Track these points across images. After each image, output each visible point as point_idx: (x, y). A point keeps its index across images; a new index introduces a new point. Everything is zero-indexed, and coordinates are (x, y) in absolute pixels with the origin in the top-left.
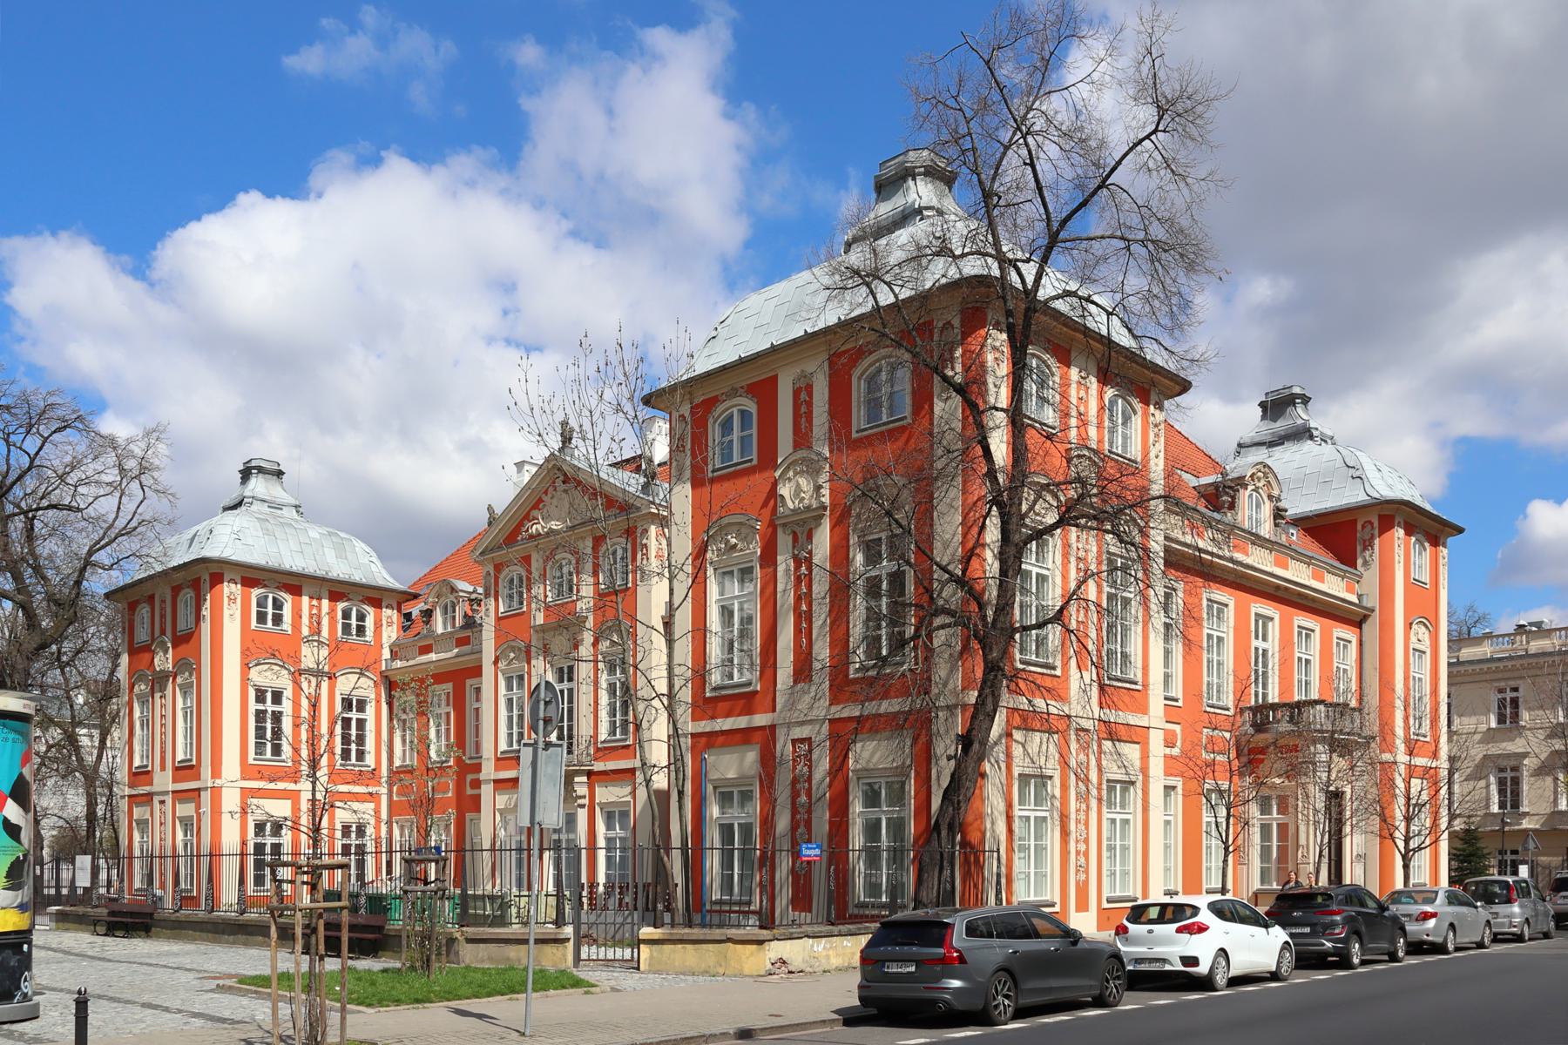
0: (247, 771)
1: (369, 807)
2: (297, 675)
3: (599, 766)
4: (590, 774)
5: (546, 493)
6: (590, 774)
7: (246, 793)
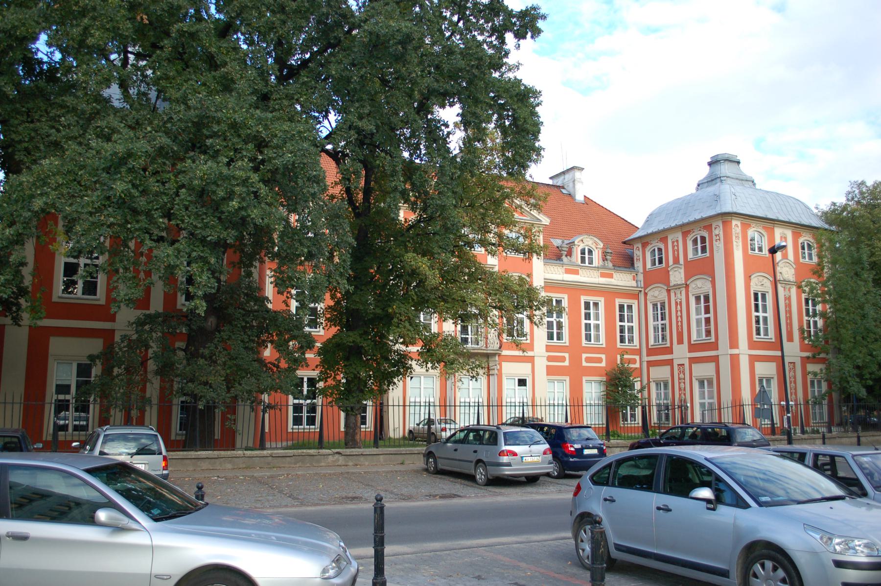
0: (752, 345)
1: (668, 368)
2: (775, 283)
3: (505, 353)
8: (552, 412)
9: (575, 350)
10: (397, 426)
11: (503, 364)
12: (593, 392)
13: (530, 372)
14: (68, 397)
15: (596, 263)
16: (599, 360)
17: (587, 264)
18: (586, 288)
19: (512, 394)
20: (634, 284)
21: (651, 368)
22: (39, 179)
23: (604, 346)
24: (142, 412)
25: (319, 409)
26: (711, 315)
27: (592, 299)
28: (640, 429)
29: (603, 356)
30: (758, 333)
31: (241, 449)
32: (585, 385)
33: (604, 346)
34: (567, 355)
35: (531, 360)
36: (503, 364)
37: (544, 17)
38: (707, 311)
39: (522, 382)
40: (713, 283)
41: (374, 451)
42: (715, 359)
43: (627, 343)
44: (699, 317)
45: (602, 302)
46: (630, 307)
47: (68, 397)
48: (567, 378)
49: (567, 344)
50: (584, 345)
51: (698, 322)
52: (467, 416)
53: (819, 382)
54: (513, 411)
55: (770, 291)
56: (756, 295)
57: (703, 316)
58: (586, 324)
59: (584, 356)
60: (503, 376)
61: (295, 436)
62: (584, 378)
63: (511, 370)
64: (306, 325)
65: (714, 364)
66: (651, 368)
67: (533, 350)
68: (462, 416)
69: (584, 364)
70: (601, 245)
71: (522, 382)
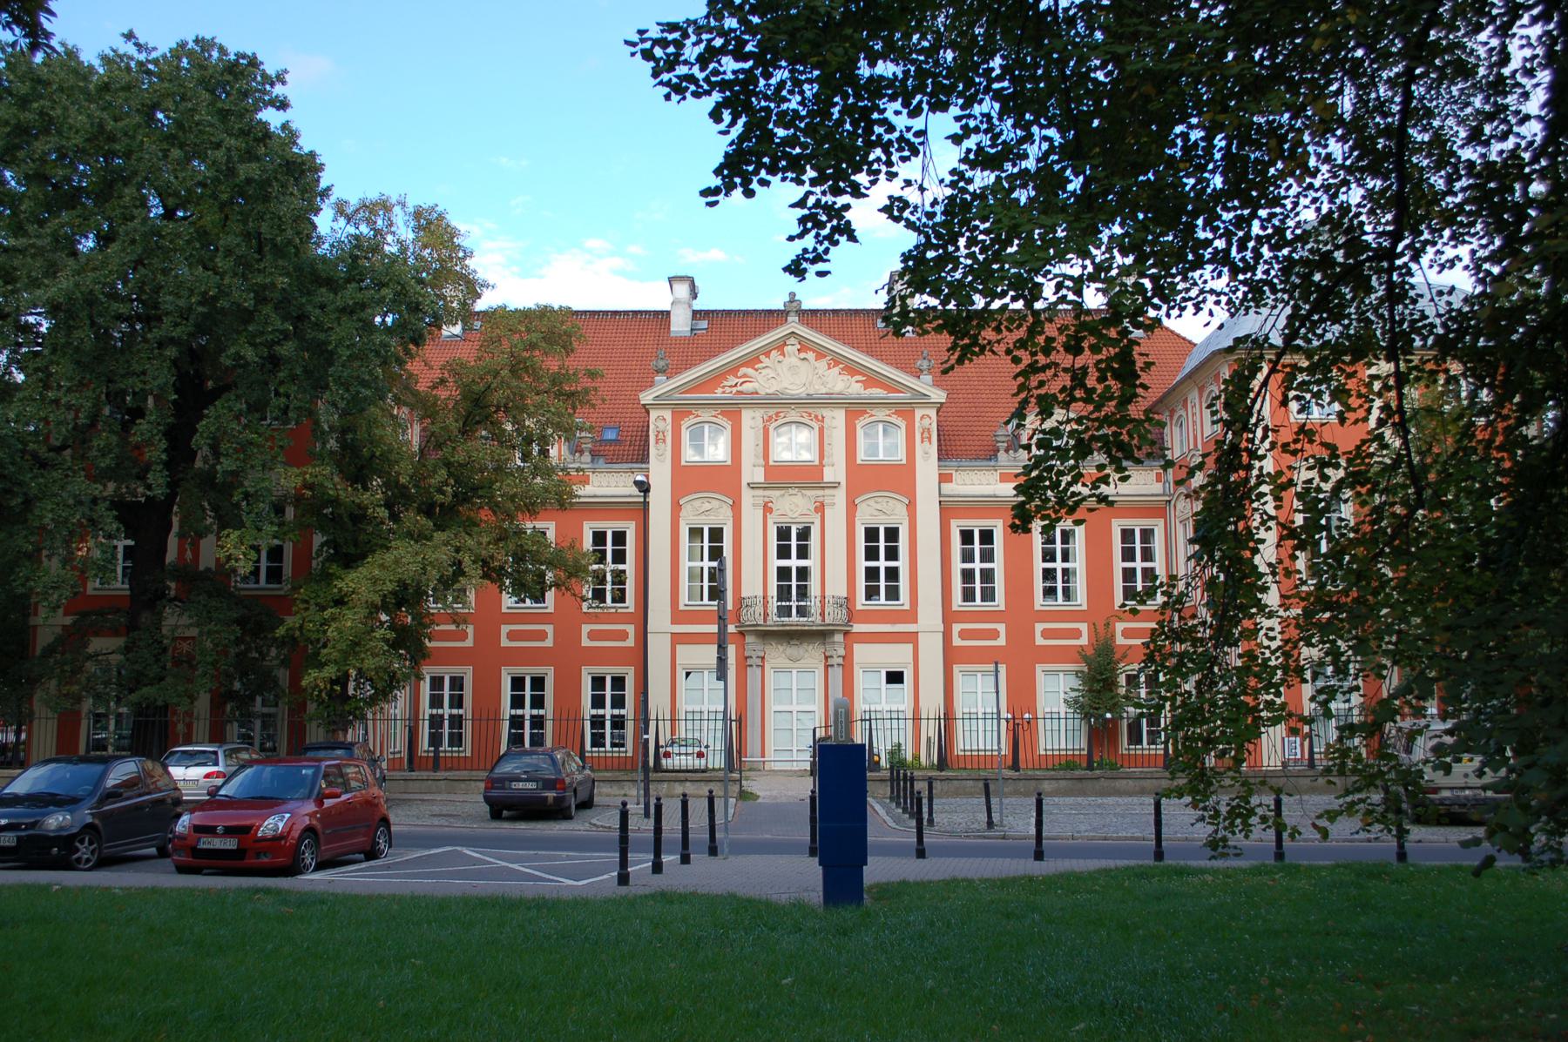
3: (858, 628)
4: (846, 633)
5: (767, 354)
6: (846, 633)
7: (677, 639)
9: (1020, 616)
12: (1055, 690)
14: (623, 712)
22: (197, 326)
23: (1085, 607)
24: (189, 726)
25: (549, 725)
32: (1040, 677)
33: (1085, 607)
34: (1001, 628)
35: (912, 638)
37: (280, 78)
39: (895, 678)
40: (911, 507)
41: (407, 774)
42: (912, 638)
46: (1147, 535)
47: (623, 712)
50: (1037, 607)
52: (974, 734)
55: (730, 523)
56: (871, 534)
58: (1125, 570)
59: (505, 629)
60: (856, 668)
61: (602, 762)
63: (872, 658)
69: (1040, 641)
71: (895, 678)
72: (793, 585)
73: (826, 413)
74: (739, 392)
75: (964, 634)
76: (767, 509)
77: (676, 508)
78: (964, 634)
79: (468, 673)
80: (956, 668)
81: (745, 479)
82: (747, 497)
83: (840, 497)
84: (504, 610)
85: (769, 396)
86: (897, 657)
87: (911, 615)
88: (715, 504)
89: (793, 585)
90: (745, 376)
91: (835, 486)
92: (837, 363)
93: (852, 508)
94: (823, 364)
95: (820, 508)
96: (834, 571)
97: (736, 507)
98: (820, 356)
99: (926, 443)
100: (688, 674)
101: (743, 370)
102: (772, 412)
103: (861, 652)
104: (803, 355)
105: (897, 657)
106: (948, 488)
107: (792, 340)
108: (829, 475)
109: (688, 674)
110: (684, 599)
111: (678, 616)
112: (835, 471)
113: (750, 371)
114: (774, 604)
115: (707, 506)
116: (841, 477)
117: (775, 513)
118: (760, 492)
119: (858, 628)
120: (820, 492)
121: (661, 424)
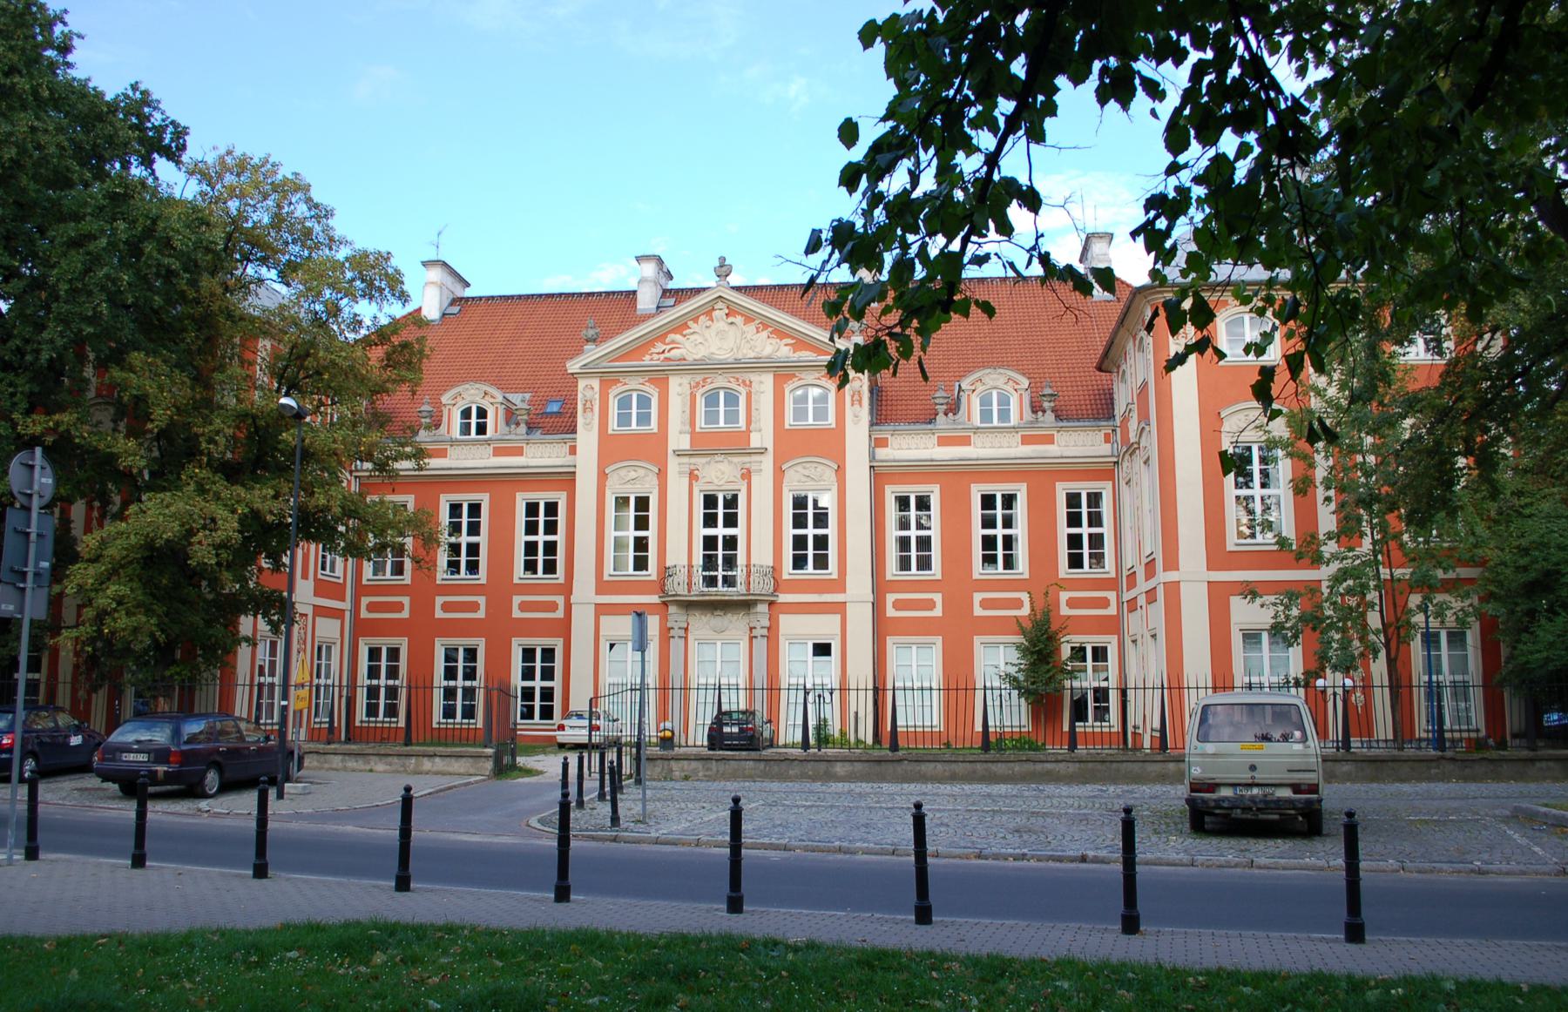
3: (783, 598)
4: (771, 603)
5: (696, 320)
6: (771, 603)
7: (601, 610)
8: (927, 703)
10: (700, 722)
11: (782, 618)
12: (996, 660)
13: (838, 631)
15: (1014, 420)
16: (1018, 604)
17: (995, 423)
18: (968, 469)
19: (798, 666)
20: (1106, 449)
21: (602, 618)
23: (1026, 576)
26: (702, 532)
27: (999, 490)
28: (1114, 739)
29: (1025, 597)
30: (323, 568)
31: (418, 744)
33: (1026, 576)
34: (938, 598)
36: (782, 618)
38: (642, 523)
40: (840, 471)
42: (840, 608)
43: (388, 575)
44: (532, 538)
45: (1022, 493)
47: (475, 683)
48: (939, 640)
49: (939, 577)
51: (619, 544)
52: (927, 710)
53: (1457, 638)
54: (734, 699)
57: (631, 533)
62: (977, 640)
63: (798, 630)
64: (244, 585)
65: (838, 617)
66: (602, 618)
67: (843, 590)
68: (701, 708)
70: (1025, 383)
71: (822, 650)
72: (719, 555)
73: (754, 377)
74: (667, 359)
75: (898, 605)
76: (693, 477)
77: (602, 477)
78: (898, 605)
79: (403, 644)
80: (890, 640)
81: (672, 446)
82: (673, 464)
83: (767, 463)
84: (516, 581)
85: (696, 362)
86: (825, 627)
87: (839, 585)
88: (641, 472)
89: (719, 555)
90: (673, 342)
91: (762, 451)
92: (766, 327)
93: (779, 474)
94: (751, 328)
95: (747, 475)
96: (762, 541)
97: (662, 475)
98: (748, 320)
99: (857, 406)
100: (612, 646)
101: (671, 337)
102: (699, 378)
103: (789, 624)
104: (731, 319)
105: (825, 627)
106: (882, 453)
107: (720, 305)
108: (755, 442)
109: (612, 646)
110: (609, 568)
111: (602, 587)
112: (763, 437)
113: (678, 337)
114: (699, 574)
115: (633, 475)
116: (769, 445)
117: (701, 481)
118: (685, 460)
119: (783, 598)
120: (747, 459)
121: (589, 394)
